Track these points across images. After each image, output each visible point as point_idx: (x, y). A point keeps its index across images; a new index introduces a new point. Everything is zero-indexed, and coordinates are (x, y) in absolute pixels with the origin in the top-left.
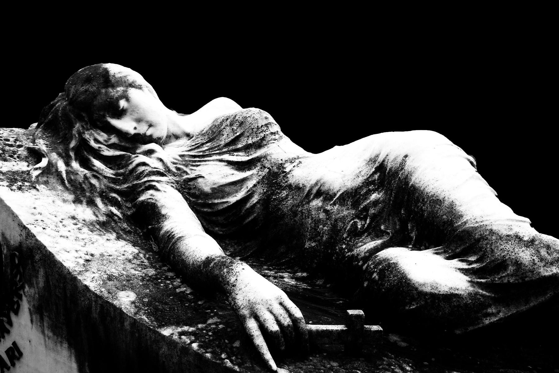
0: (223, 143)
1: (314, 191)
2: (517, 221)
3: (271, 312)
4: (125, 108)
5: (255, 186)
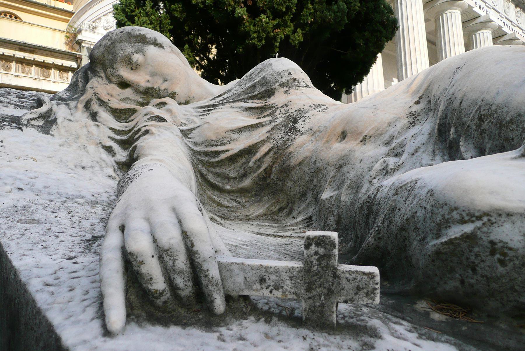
3: (148, 220)
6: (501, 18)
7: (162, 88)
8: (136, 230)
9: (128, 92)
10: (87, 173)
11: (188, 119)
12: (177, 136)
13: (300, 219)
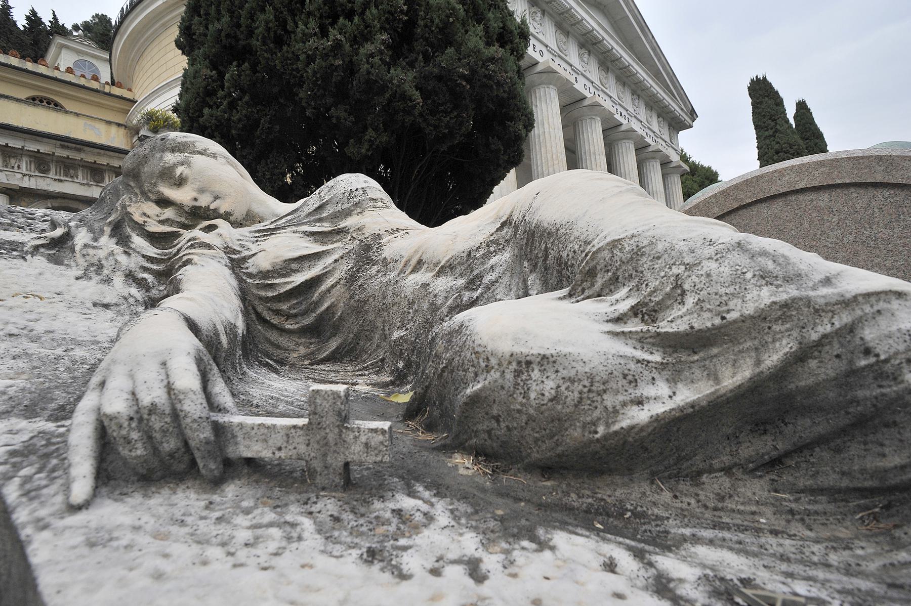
0: (304, 214)
1: (414, 262)
2: (687, 221)
4: (184, 175)
5: (336, 261)
6: (643, 128)
7: (212, 207)
9: (169, 213)
11: (242, 246)
12: (226, 266)
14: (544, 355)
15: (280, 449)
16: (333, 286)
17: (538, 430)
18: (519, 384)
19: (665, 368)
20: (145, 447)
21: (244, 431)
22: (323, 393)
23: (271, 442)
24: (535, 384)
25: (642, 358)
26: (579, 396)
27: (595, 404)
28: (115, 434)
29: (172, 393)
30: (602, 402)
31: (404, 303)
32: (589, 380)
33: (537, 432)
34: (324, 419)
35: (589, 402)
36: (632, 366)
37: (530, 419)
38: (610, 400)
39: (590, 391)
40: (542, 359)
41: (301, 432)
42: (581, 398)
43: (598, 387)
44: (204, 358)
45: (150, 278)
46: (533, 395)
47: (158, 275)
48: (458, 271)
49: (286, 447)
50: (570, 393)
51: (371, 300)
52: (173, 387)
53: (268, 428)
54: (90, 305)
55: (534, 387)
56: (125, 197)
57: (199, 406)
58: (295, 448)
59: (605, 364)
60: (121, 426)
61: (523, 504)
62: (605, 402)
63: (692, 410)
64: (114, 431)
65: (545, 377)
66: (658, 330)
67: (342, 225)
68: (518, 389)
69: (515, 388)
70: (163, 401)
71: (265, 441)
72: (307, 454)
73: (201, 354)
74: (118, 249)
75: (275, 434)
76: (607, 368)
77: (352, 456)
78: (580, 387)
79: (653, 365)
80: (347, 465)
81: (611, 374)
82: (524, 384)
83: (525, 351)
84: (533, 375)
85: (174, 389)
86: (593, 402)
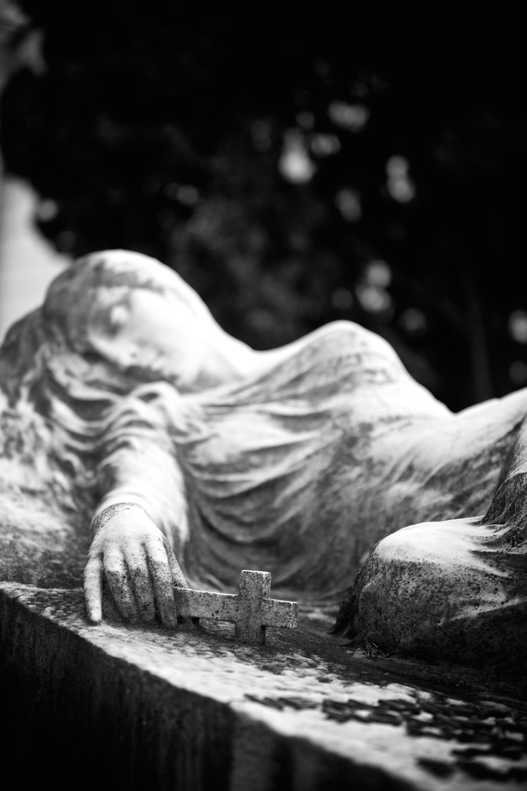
1: (403, 467)
3: (123, 552)
5: (309, 457)
8: (113, 557)
10: (111, 519)
11: (190, 425)
13: (334, 592)
14: (414, 563)
15: (217, 612)
16: (302, 490)
17: (403, 619)
18: (393, 583)
19: (510, 583)
20: (130, 597)
21: (194, 598)
22: (251, 574)
23: (211, 607)
24: (403, 584)
25: (491, 573)
26: (431, 594)
27: (442, 601)
28: (114, 585)
29: (150, 563)
30: (446, 600)
31: (382, 519)
32: (441, 584)
33: (403, 621)
34: (250, 593)
35: (437, 599)
36: (480, 578)
37: (398, 610)
38: (452, 599)
39: (439, 591)
40: (412, 566)
41: (234, 601)
42: (432, 596)
43: (445, 588)
44: (167, 546)
45: (75, 461)
46: (400, 592)
47: (83, 456)
48: (450, 482)
49: (222, 611)
50: (425, 592)
51: (345, 512)
52: (151, 560)
53: (211, 596)
54: (17, 490)
55: (402, 586)
56: (45, 349)
57: (167, 574)
58: (228, 612)
59: (457, 573)
60: (118, 581)
61: (387, 674)
62: (449, 600)
63: (511, 612)
64: (114, 583)
65: (411, 579)
66: (508, 553)
67: (325, 405)
68: (392, 587)
69: (390, 586)
70: (144, 568)
71: (208, 605)
72: (236, 617)
73: (166, 542)
74: (39, 420)
75: (216, 601)
76: (456, 576)
77: (266, 621)
78: (433, 588)
79: (500, 579)
80: (264, 628)
81: (459, 580)
82: (397, 583)
83: (402, 559)
84: (403, 578)
85: (151, 561)
86: (440, 599)
